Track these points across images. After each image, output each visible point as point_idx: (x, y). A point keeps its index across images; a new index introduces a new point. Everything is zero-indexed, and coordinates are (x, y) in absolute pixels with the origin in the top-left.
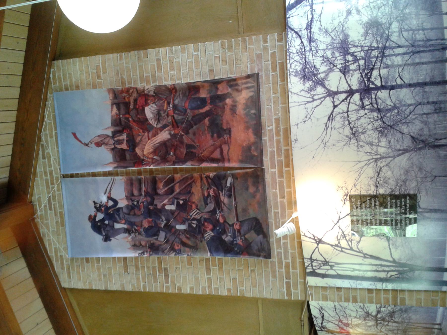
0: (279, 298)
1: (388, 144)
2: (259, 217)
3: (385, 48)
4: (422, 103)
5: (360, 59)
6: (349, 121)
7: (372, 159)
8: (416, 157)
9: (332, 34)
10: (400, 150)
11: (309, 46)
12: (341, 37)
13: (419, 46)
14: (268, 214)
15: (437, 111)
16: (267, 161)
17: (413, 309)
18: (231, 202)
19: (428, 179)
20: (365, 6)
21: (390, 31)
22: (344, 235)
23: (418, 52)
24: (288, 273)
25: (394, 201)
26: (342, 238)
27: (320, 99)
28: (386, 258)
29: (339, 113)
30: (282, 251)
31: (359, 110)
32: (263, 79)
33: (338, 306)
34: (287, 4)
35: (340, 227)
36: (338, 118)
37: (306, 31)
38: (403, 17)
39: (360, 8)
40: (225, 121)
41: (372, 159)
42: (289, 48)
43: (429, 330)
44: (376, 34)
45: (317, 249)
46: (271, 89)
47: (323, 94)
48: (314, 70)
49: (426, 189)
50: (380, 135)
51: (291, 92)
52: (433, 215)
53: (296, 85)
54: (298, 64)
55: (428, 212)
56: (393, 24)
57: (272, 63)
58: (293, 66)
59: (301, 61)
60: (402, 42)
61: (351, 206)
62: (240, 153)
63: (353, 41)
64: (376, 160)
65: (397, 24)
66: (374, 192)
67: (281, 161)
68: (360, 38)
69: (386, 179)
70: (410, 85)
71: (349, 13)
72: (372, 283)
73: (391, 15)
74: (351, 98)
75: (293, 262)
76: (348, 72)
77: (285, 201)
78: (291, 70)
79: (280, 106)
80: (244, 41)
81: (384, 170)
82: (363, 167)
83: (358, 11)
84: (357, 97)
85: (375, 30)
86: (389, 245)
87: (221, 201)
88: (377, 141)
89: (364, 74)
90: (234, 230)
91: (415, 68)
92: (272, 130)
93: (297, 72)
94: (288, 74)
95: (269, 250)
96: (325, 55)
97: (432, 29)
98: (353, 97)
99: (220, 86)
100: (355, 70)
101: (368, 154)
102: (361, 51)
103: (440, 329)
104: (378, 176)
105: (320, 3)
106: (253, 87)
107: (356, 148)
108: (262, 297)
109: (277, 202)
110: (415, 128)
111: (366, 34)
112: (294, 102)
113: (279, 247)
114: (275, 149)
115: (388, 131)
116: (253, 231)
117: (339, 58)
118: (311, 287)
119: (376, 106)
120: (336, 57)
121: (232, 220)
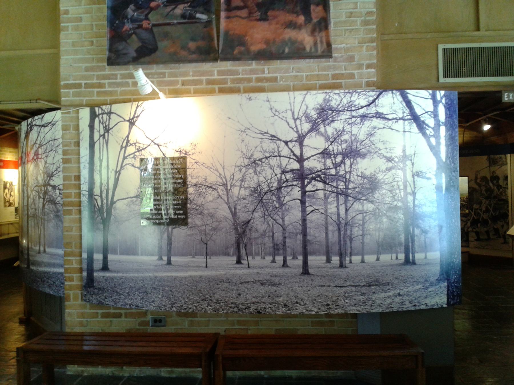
0: (62, 74)
1: (242, 197)
2: (158, 53)
3: (347, 195)
4: (285, 232)
5: (336, 169)
6: (269, 157)
7: (226, 181)
8: (227, 224)
9: (367, 140)
10: (235, 209)
11: (357, 115)
12: (363, 150)
13: (346, 230)
14: (162, 65)
15: (276, 247)
16: (227, 65)
17: (60, 223)
18: (176, 17)
19: (204, 237)
20: (395, 176)
21: (365, 201)
22: (141, 150)
23: (339, 229)
24: (92, 86)
25: (180, 202)
26: (137, 147)
27: (296, 126)
28: (116, 194)
29: (278, 147)
30: (119, 80)
31: (280, 168)
32: (324, 63)
33: (57, 143)
34: (408, 91)
35: (149, 145)
36: (273, 146)
37: (375, 112)
38: (379, 216)
39: (393, 171)
40: (277, 13)
41: (226, 181)
42: (358, 92)
43: (38, 240)
44: (362, 187)
45: (123, 120)
46: (312, 73)
47: (302, 130)
48: (329, 121)
49: (193, 234)
50: (253, 189)
51: (306, 95)
52: (165, 242)
53: (315, 99)
54: (338, 103)
55: (168, 237)
56: (372, 205)
57: (343, 74)
58: (336, 97)
59: (341, 105)
60: (352, 213)
61: (173, 159)
62: (237, 32)
63: (357, 163)
64: (225, 185)
65: (371, 209)
66: (190, 182)
67: (226, 83)
68: (360, 170)
69: (204, 195)
70: (304, 220)
71: (389, 159)
72: (87, 180)
73: (382, 203)
74: (295, 160)
75: (106, 93)
76: (324, 157)
77: (179, 86)
78: (331, 94)
79: (292, 84)
80: (372, 41)
81: (215, 193)
82: (218, 171)
83: (389, 169)
84: (296, 166)
85: (368, 186)
86: (131, 198)
87: (177, 5)
88: (246, 186)
89: (319, 173)
90: (141, 21)
91: (322, 225)
92: (264, 72)
93: (329, 101)
94: (328, 91)
95: (118, 64)
96: (345, 133)
97: (363, 243)
98: (295, 162)
99: (320, 8)
100: (325, 164)
101: (232, 177)
102: (345, 171)
103: (39, 252)
104: (208, 187)
105: (404, 128)
106: (317, 50)
107: (238, 164)
108: (61, 54)
109: (176, 77)
110: (259, 223)
111: (364, 177)
112: (294, 98)
113: (124, 77)
114: (240, 76)
115: (256, 197)
116: (140, 44)
117: (340, 148)
118: (78, 112)
119: (284, 185)
120: (341, 145)
121: (154, 18)
